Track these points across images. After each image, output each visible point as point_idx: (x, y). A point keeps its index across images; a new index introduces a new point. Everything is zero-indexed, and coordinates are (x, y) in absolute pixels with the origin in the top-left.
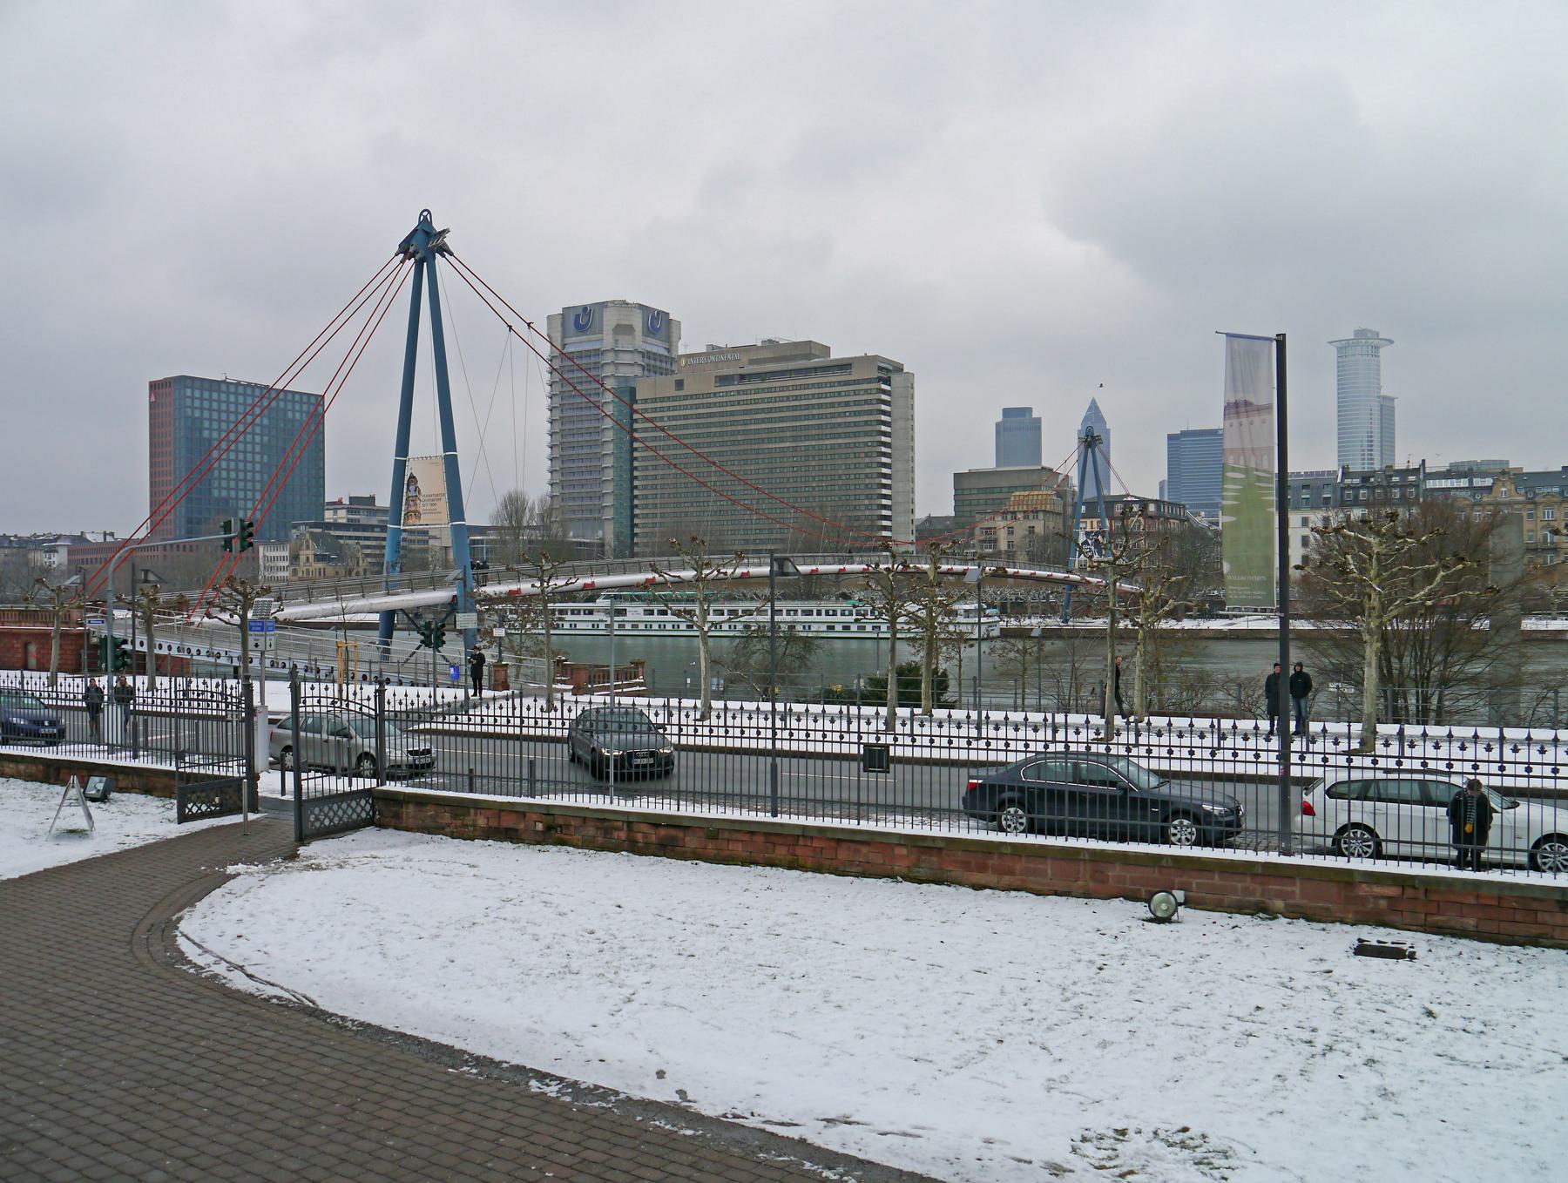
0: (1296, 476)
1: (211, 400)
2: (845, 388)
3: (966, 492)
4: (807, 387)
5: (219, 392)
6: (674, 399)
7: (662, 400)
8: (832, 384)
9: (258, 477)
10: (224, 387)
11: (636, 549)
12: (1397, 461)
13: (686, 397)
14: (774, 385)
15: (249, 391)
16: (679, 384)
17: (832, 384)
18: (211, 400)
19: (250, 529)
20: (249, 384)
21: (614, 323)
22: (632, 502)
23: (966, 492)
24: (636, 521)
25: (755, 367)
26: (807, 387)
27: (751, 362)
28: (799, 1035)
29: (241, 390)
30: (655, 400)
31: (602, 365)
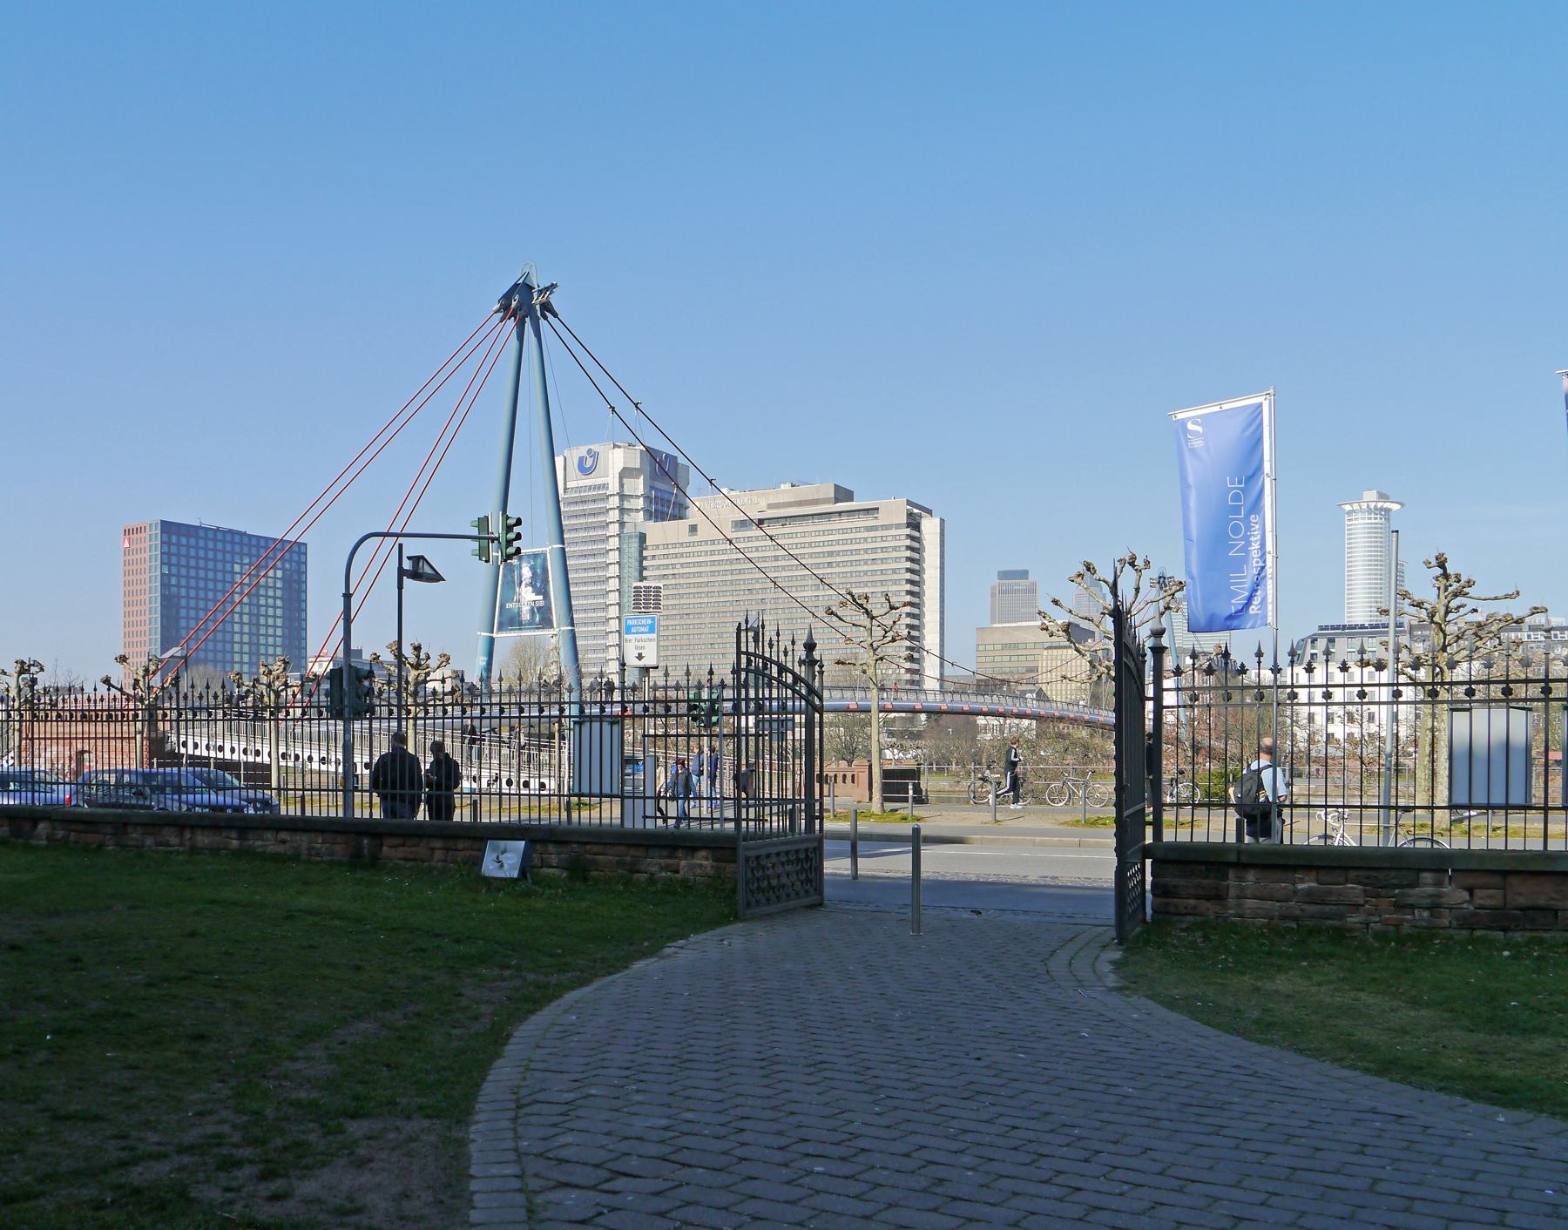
0: (1360, 628)
1: (188, 546)
2: (872, 534)
3: (989, 647)
4: (830, 532)
5: (198, 538)
6: (688, 545)
7: (674, 545)
8: (858, 530)
9: (237, 628)
10: (202, 533)
11: (645, 573)
12: (622, 455)
13: (700, 543)
14: (794, 530)
15: (228, 537)
16: (693, 529)
17: (858, 530)
18: (188, 546)
19: (516, 530)
20: (231, 531)
21: (619, 466)
22: (641, 562)
23: (989, 647)
24: (645, 563)
25: (775, 511)
26: (830, 532)
27: (770, 506)
28: (685, 668)
29: (220, 536)
30: (667, 546)
31: (607, 524)
